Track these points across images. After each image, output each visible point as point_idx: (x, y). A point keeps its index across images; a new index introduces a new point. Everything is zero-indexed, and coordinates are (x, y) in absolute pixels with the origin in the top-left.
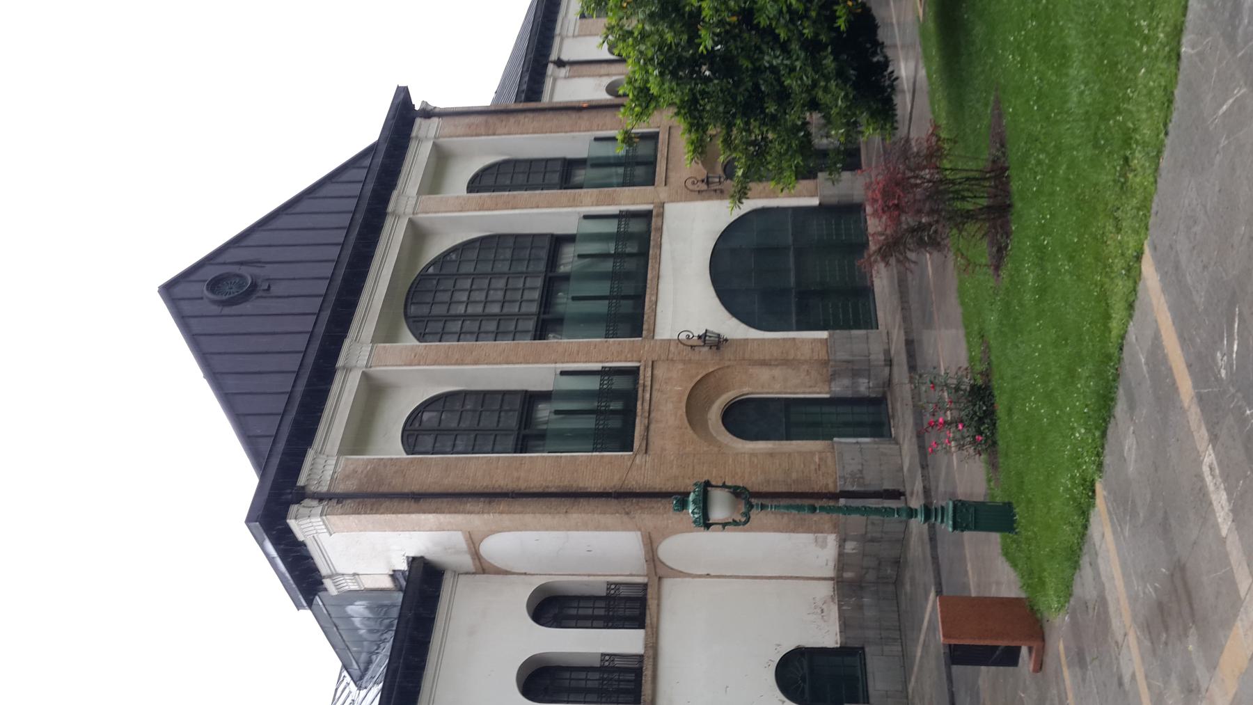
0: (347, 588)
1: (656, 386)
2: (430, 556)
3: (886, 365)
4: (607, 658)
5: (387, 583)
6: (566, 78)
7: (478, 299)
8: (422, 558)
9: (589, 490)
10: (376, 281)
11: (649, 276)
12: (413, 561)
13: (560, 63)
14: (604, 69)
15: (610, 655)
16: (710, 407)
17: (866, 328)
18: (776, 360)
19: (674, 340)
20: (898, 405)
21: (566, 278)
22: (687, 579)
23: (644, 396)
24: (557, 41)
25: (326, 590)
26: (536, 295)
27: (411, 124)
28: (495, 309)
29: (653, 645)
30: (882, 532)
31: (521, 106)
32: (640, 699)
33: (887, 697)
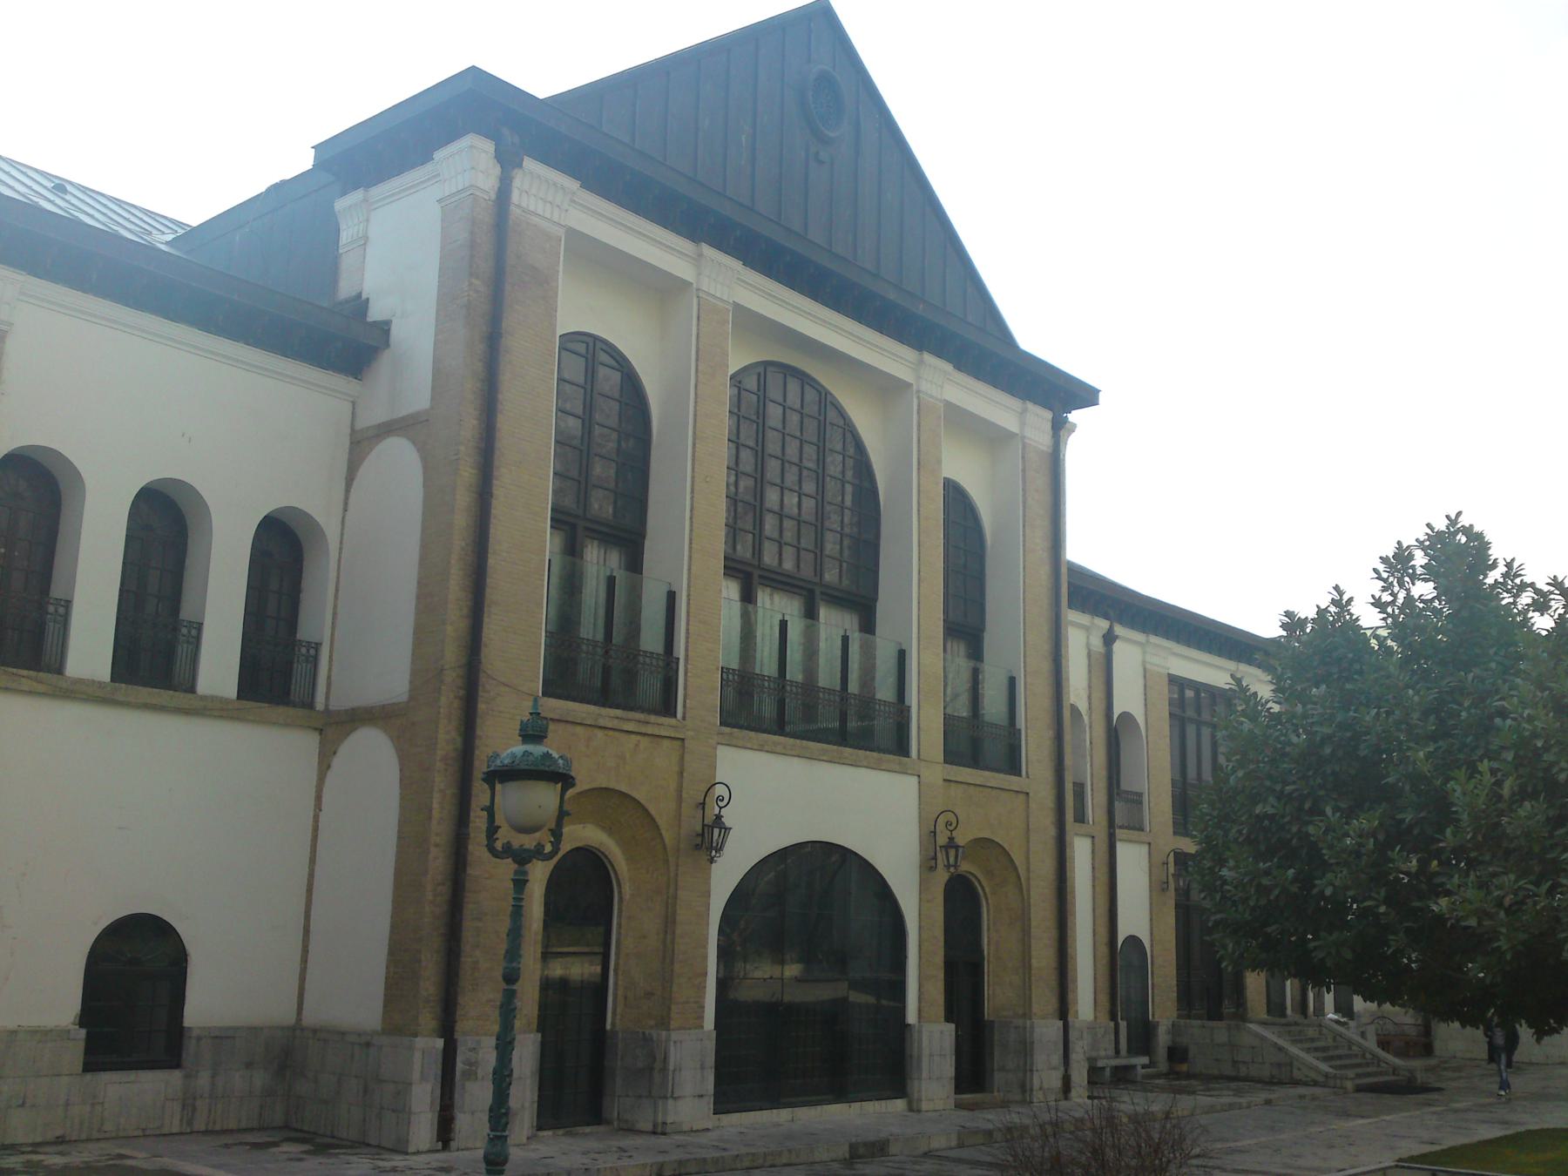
0: (345, 227)
1: (645, 741)
2: (384, 362)
3: (655, 1126)
4: (194, 632)
5: (345, 289)
6: (1088, 645)
7: (787, 475)
8: (387, 344)
9: (486, 620)
10: (824, 323)
11: (811, 744)
12: (384, 328)
13: (1109, 639)
14: (1099, 706)
15: (198, 638)
16: (603, 828)
17: (716, 1095)
18: (673, 942)
19: (714, 777)
20: (593, 1144)
21: (810, 613)
22: (315, 778)
23: (631, 720)
24: (1140, 637)
25: (344, 193)
26: (788, 565)
27: (1046, 405)
28: (772, 497)
29: (213, 709)
30: (382, 1108)
31: (1064, 570)
32: (121, 682)
33: (93, 1105)
